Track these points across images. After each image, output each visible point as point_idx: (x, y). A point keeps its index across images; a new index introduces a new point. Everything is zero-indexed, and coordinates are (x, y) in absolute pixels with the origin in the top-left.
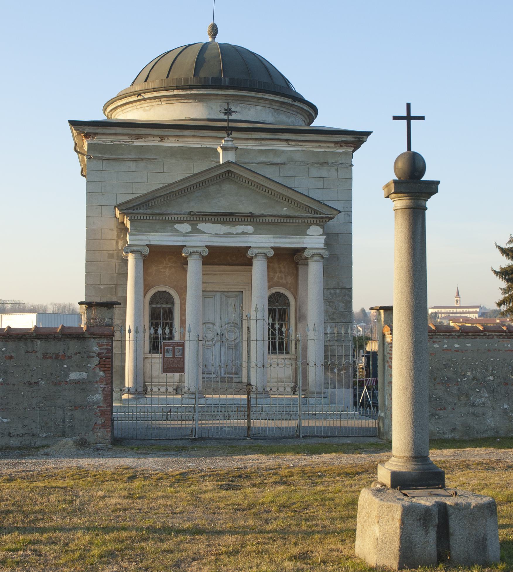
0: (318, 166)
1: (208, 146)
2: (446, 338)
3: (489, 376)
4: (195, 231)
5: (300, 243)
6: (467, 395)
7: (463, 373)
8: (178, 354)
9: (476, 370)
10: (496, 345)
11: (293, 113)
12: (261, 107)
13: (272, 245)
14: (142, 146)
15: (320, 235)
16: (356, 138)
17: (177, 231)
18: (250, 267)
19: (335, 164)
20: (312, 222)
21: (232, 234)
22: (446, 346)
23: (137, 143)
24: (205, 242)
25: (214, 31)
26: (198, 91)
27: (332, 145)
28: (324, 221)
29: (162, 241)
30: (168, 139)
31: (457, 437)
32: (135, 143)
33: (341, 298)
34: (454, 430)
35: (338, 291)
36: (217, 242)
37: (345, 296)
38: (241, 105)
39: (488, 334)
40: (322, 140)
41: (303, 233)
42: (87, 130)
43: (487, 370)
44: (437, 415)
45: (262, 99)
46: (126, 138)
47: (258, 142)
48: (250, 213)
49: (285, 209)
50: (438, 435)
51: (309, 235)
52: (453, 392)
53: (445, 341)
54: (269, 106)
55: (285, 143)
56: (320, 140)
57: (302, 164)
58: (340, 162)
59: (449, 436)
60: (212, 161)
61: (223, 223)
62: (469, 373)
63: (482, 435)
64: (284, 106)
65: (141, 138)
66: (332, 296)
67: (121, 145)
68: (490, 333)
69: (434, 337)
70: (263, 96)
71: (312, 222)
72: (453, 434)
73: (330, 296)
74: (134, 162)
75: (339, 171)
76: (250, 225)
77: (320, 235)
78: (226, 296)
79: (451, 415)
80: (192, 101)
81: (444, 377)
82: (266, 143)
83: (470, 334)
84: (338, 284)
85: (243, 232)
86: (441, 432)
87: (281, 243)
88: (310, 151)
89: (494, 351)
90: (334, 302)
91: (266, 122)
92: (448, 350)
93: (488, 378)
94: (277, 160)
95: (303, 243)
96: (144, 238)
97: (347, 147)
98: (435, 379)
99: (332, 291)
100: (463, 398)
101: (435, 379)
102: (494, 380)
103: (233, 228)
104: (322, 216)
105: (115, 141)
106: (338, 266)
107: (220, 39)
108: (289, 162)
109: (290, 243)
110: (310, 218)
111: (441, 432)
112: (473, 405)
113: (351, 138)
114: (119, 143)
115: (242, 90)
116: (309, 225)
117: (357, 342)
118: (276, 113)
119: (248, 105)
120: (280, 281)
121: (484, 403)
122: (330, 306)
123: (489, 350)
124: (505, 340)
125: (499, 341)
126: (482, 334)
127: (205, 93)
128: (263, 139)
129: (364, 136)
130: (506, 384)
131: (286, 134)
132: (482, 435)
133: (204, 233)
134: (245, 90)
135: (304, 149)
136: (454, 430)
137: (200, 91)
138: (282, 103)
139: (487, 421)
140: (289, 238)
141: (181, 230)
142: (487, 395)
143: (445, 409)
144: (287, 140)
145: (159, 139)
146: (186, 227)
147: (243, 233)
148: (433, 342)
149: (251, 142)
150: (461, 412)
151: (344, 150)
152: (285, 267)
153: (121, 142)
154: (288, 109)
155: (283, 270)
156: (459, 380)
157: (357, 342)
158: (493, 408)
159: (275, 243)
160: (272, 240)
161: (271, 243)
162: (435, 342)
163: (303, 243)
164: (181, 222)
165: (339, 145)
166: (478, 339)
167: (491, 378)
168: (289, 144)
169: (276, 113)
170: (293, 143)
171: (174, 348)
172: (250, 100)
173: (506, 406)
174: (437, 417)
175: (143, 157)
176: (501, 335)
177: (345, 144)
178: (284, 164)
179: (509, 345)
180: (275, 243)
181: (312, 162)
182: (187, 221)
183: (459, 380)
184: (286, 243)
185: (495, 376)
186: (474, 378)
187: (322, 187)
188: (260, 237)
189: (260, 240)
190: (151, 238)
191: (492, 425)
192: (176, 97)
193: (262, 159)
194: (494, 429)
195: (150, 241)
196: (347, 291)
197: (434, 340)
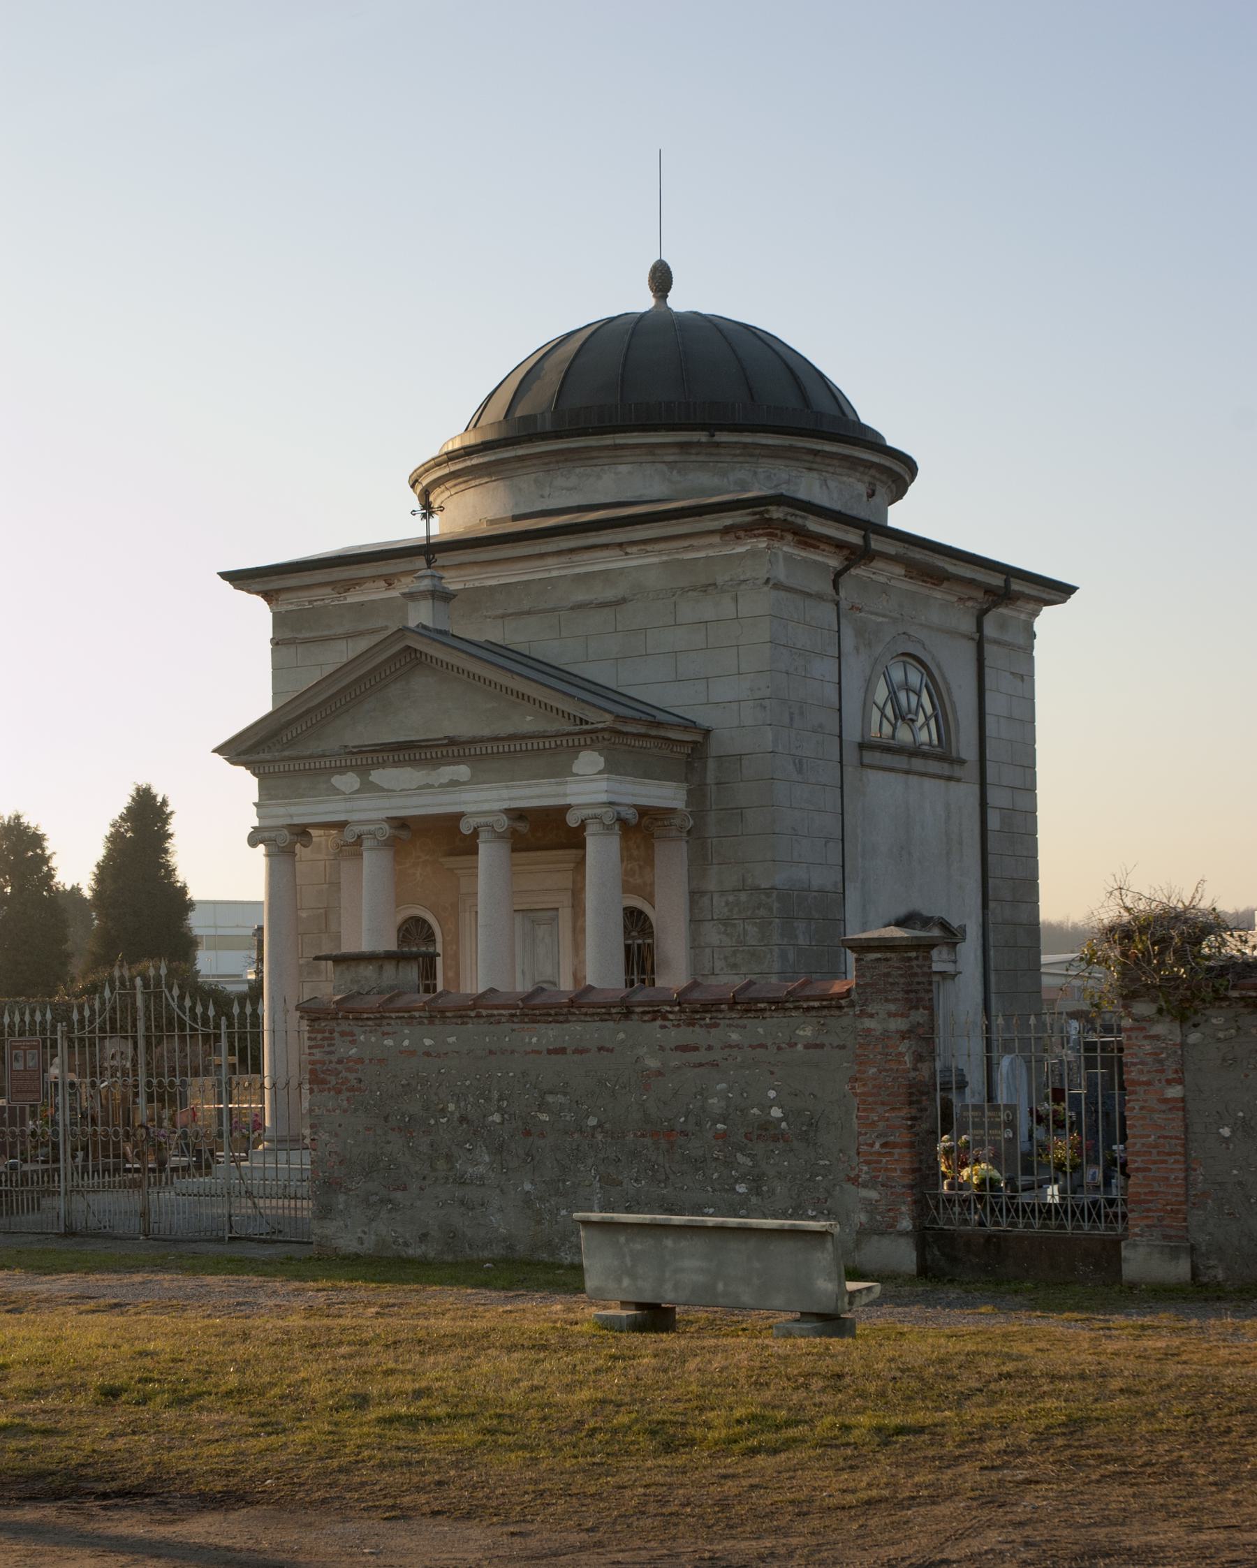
0: (695, 594)
1: (477, 584)
2: (408, 1024)
3: (492, 1114)
4: (368, 787)
5: (558, 795)
6: (449, 1158)
7: (441, 1106)
8: (31, 1064)
9: (465, 1100)
10: (507, 1039)
11: (741, 459)
12: (630, 466)
13: (506, 805)
14: (362, 604)
15: (600, 773)
16: (755, 514)
17: (336, 791)
18: (474, 857)
19: (730, 583)
20: (582, 743)
21: (431, 786)
22: (406, 1043)
23: (353, 598)
24: (384, 809)
25: (661, 279)
26: (481, 457)
27: (716, 539)
28: (600, 738)
29: (311, 814)
30: (399, 581)
31: (432, 1254)
32: (349, 600)
33: (749, 913)
34: (424, 1237)
35: (743, 897)
36: (408, 808)
37: (759, 908)
38: (577, 470)
39: (484, 1012)
40: (507, 556)
41: (562, 771)
42: (276, 583)
43: (488, 1100)
44: (390, 1201)
45: (617, 447)
46: (328, 590)
47: (563, 559)
48: (445, 738)
49: (529, 718)
50: (395, 1247)
51: (578, 775)
52: (420, 1148)
53: (407, 1031)
54: (650, 458)
55: (617, 552)
56: (676, 533)
57: (661, 596)
58: (742, 578)
59: (414, 1251)
60: (486, 617)
61: (414, 763)
62: (451, 1107)
63: (480, 1253)
64: (693, 451)
65: (354, 586)
66: (731, 911)
67: (326, 606)
68: (490, 1012)
69: (385, 1022)
70: (619, 441)
71: (582, 743)
72: (423, 1247)
73: (726, 910)
74: (349, 640)
75: (740, 600)
76: (463, 763)
77: (600, 773)
78: (533, 921)
79: (418, 1203)
80: (486, 480)
81: (403, 1116)
82: (579, 559)
83: (448, 1014)
84: (743, 881)
85: (451, 780)
86: (401, 1240)
87: (521, 798)
88: (678, 560)
89: (503, 1053)
90: (734, 925)
91: (645, 499)
92: (411, 1053)
93: (490, 1119)
94: (610, 594)
95: (565, 795)
96: (281, 811)
97: (751, 537)
98: (386, 1119)
99: (731, 898)
100: (441, 1164)
101: (386, 1119)
102: (502, 1123)
103: (433, 773)
104: (585, 727)
105: (316, 601)
106: (742, 835)
107: (679, 301)
108: (635, 595)
109: (539, 797)
110: (548, 737)
111: (401, 1240)
112: (461, 1181)
113: (742, 516)
114: (322, 603)
115: (562, 438)
116: (575, 750)
117: (48, 1041)
118: (675, 472)
119: (595, 469)
120: (631, 880)
121: (482, 1178)
122: (727, 935)
123: (491, 1052)
124: (526, 1026)
125: (513, 1030)
126: (473, 1014)
127: (493, 458)
128: (572, 551)
129: (770, 508)
130: (528, 1133)
131: (605, 532)
132: (480, 1253)
133: (382, 789)
134: (568, 437)
135: (665, 558)
136: (424, 1237)
137: (484, 456)
138: (683, 446)
139: (491, 1221)
140: (537, 785)
141: (343, 788)
142: (487, 1158)
143: (405, 1189)
144: (620, 545)
145: (383, 584)
146: (348, 782)
147: (454, 783)
148: (384, 1034)
149: (551, 561)
150: (437, 1197)
151: (749, 548)
152: (638, 847)
153: (327, 601)
154: (711, 454)
155: (635, 853)
156: (432, 1122)
157: (48, 1041)
158: (502, 1190)
159: (510, 799)
160: (505, 793)
161: (504, 800)
162: (388, 1034)
163: (565, 795)
164: (341, 770)
165: (732, 536)
166: (470, 1026)
167: (496, 1118)
168: (627, 554)
169: (675, 472)
170: (634, 549)
171: (25, 1051)
172: (595, 454)
173: (528, 1187)
174: (390, 1206)
175: (363, 627)
176: (513, 1015)
177: (746, 531)
178: (623, 601)
179: (534, 1040)
180: (510, 799)
181: (683, 588)
182: (351, 768)
183: (432, 1122)
184: (531, 797)
185: (506, 1113)
186: (463, 1119)
187: (704, 646)
188: (482, 790)
189: (301, 809)
190: (293, 810)
191: (501, 1230)
192: (459, 476)
193: (581, 596)
194: (504, 1240)
195: (291, 816)
196: (763, 897)
197: (387, 1029)
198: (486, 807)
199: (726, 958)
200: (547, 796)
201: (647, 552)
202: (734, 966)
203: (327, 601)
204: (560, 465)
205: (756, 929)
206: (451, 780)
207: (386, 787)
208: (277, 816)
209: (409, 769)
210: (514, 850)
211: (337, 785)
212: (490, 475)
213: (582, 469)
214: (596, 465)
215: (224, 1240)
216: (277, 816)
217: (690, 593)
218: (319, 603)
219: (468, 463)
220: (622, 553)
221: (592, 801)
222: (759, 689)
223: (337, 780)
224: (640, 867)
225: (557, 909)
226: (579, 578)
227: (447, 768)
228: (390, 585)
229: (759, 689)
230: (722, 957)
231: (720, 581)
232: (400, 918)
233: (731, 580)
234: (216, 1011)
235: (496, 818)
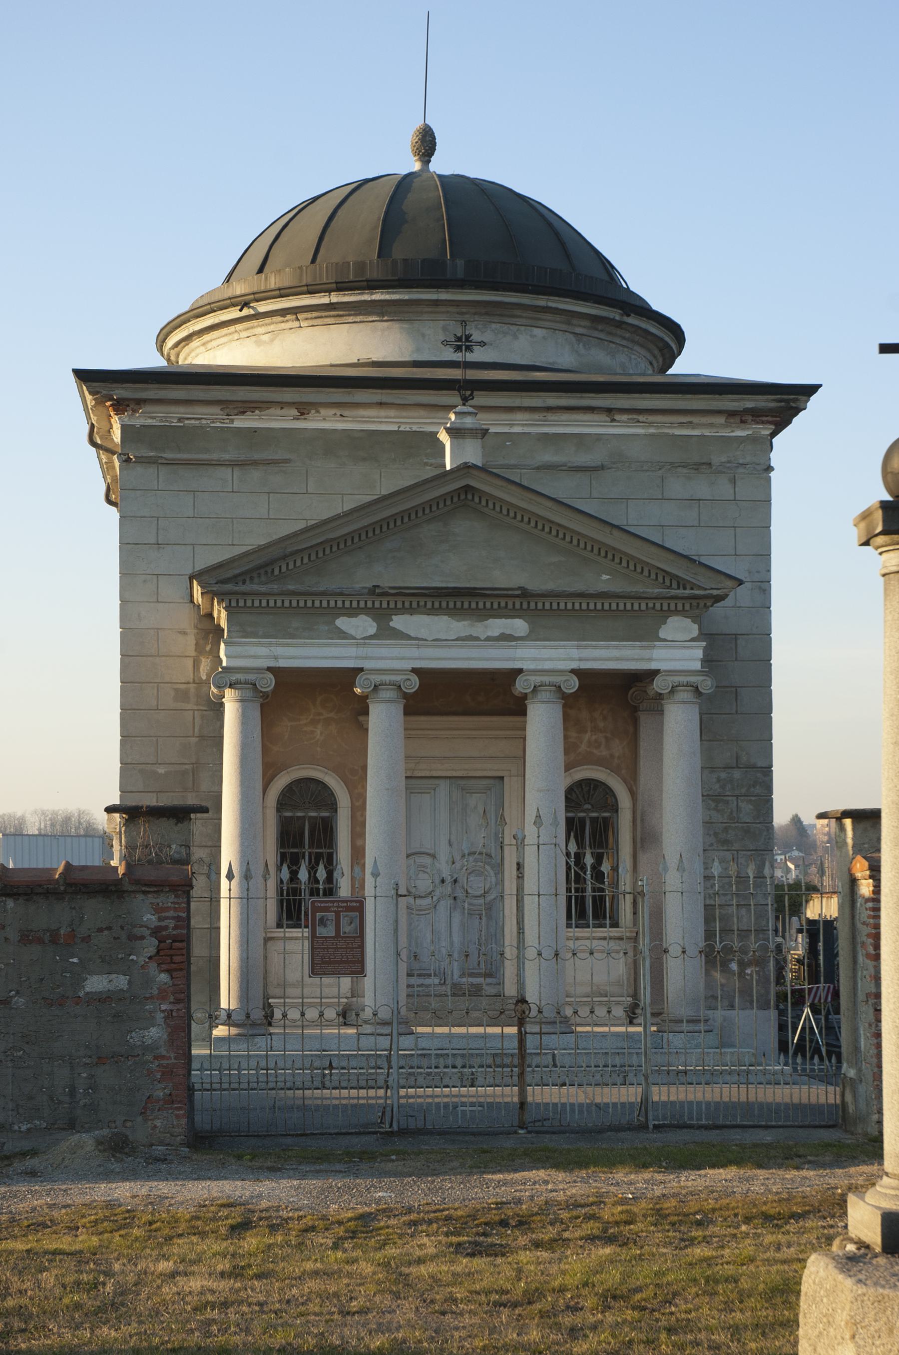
0: (685, 470)
1: (415, 428)
4: (386, 633)
5: (642, 659)
11: (624, 343)
13: (574, 665)
14: (255, 430)
15: (693, 640)
16: (780, 401)
17: (343, 635)
19: (728, 465)
21: (477, 639)
23: (241, 422)
26: (388, 293)
30: (318, 412)
32: (238, 424)
33: (743, 791)
35: (737, 774)
37: (754, 786)
38: (494, 326)
41: (650, 635)
42: (120, 392)
46: (216, 410)
48: (520, 588)
54: (564, 327)
55: (603, 417)
57: (645, 468)
58: (741, 461)
61: (456, 612)
67: (202, 427)
70: (551, 304)
71: (673, 607)
73: (717, 786)
74: (236, 469)
75: (738, 483)
76: (519, 617)
78: (463, 789)
82: (556, 418)
84: (737, 758)
88: (667, 435)
90: (727, 802)
91: (556, 366)
94: (584, 459)
95: (650, 660)
97: (758, 423)
99: (723, 775)
103: (479, 624)
105: (188, 419)
107: (441, 165)
108: (614, 463)
109: (618, 659)
113: (767, 401)
116: (664, 616)
118: (581, 345)
119: (512, 327)
120: (595, 751)
122: (718, 811)
128: (549, 409)
129: (800, 397)
133: (409, 637)
134: (504, 290)
135: (652, 431)
137: (393, 293)
138: (596, 320)
141: (352, 632)
144: (609, 411)
145: (295, 412)
146: (364, 625)
149: (520, 416)
151: (750, 432)
152: (605, 718)
153: (204, 422)
154: (610, 333)
155: (601, 725)
159: (580, 660)
160: (575, 653)
163: (650, 660)
164: (352, 612)
165: (737, 419)
168: (613, 420)
172: (518, 312)
175: (256, 456)
177: (753, 416)
178: (602, 467)
180: (580, 660)
181: (672, 463)
182: (366, 611)
188: (545, 647)
189: (292, 651)
195: (276, 658)
196: (759, 775)
198: (548, 665)
199: (716, 834)
200: (628, 660)
201: (639, 422)
202: (726, 842)
203: (204, 422)
204: (476, 317)
205: (751, 807)
206: (503, 634)
207: (412, 635)
208: (255, 657)
209: (446, 618)
210: (406, 713)
211: (344, 628)
212: (382, 314)
213: (499, 325)
214: (512, 324)
215: (648, 1127)
216: (255, 657)
217: (680, 469)
218: (193, 422)
219: (366, 297)
220: (608, 419)
221: (681, 668)
222: (758, 572)
223: (342, 622)
224: (606, 738)
225: (502, 778)
226: (546, 438)
227: (498, 621)
228: (302, 414)
229: (758, 572)
230: (712, 833)
231: (716, 460)
232: (568, 782)
233: (729, 462)
234: (793, 864)
235: (564, 678)
